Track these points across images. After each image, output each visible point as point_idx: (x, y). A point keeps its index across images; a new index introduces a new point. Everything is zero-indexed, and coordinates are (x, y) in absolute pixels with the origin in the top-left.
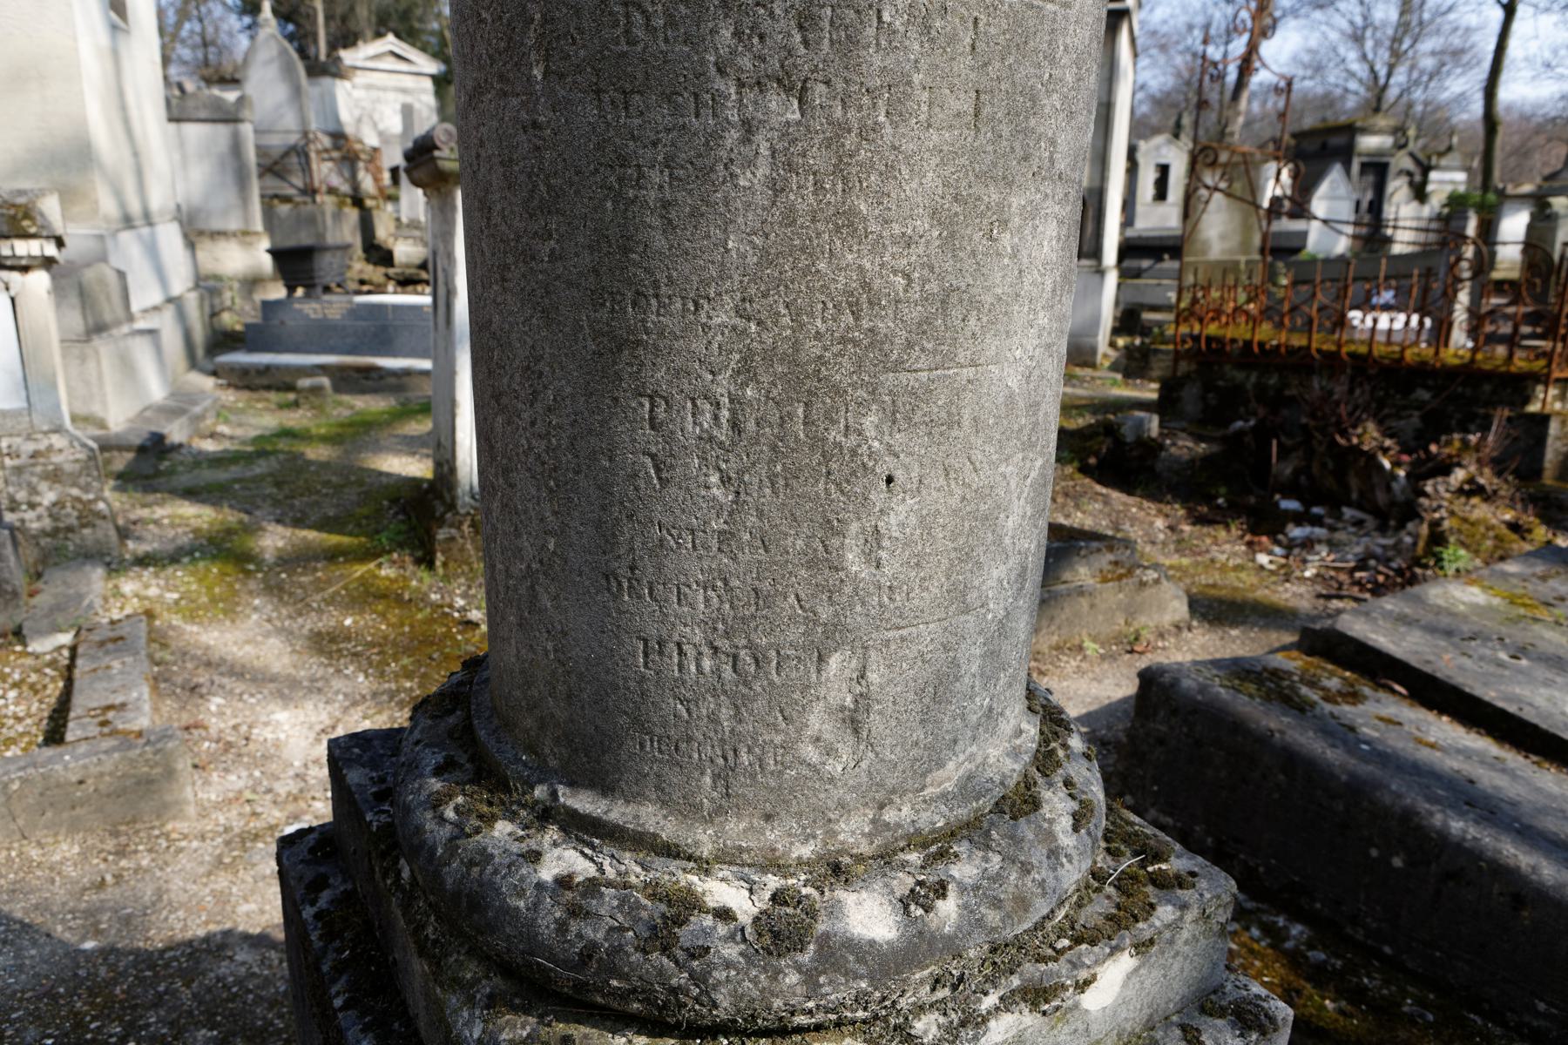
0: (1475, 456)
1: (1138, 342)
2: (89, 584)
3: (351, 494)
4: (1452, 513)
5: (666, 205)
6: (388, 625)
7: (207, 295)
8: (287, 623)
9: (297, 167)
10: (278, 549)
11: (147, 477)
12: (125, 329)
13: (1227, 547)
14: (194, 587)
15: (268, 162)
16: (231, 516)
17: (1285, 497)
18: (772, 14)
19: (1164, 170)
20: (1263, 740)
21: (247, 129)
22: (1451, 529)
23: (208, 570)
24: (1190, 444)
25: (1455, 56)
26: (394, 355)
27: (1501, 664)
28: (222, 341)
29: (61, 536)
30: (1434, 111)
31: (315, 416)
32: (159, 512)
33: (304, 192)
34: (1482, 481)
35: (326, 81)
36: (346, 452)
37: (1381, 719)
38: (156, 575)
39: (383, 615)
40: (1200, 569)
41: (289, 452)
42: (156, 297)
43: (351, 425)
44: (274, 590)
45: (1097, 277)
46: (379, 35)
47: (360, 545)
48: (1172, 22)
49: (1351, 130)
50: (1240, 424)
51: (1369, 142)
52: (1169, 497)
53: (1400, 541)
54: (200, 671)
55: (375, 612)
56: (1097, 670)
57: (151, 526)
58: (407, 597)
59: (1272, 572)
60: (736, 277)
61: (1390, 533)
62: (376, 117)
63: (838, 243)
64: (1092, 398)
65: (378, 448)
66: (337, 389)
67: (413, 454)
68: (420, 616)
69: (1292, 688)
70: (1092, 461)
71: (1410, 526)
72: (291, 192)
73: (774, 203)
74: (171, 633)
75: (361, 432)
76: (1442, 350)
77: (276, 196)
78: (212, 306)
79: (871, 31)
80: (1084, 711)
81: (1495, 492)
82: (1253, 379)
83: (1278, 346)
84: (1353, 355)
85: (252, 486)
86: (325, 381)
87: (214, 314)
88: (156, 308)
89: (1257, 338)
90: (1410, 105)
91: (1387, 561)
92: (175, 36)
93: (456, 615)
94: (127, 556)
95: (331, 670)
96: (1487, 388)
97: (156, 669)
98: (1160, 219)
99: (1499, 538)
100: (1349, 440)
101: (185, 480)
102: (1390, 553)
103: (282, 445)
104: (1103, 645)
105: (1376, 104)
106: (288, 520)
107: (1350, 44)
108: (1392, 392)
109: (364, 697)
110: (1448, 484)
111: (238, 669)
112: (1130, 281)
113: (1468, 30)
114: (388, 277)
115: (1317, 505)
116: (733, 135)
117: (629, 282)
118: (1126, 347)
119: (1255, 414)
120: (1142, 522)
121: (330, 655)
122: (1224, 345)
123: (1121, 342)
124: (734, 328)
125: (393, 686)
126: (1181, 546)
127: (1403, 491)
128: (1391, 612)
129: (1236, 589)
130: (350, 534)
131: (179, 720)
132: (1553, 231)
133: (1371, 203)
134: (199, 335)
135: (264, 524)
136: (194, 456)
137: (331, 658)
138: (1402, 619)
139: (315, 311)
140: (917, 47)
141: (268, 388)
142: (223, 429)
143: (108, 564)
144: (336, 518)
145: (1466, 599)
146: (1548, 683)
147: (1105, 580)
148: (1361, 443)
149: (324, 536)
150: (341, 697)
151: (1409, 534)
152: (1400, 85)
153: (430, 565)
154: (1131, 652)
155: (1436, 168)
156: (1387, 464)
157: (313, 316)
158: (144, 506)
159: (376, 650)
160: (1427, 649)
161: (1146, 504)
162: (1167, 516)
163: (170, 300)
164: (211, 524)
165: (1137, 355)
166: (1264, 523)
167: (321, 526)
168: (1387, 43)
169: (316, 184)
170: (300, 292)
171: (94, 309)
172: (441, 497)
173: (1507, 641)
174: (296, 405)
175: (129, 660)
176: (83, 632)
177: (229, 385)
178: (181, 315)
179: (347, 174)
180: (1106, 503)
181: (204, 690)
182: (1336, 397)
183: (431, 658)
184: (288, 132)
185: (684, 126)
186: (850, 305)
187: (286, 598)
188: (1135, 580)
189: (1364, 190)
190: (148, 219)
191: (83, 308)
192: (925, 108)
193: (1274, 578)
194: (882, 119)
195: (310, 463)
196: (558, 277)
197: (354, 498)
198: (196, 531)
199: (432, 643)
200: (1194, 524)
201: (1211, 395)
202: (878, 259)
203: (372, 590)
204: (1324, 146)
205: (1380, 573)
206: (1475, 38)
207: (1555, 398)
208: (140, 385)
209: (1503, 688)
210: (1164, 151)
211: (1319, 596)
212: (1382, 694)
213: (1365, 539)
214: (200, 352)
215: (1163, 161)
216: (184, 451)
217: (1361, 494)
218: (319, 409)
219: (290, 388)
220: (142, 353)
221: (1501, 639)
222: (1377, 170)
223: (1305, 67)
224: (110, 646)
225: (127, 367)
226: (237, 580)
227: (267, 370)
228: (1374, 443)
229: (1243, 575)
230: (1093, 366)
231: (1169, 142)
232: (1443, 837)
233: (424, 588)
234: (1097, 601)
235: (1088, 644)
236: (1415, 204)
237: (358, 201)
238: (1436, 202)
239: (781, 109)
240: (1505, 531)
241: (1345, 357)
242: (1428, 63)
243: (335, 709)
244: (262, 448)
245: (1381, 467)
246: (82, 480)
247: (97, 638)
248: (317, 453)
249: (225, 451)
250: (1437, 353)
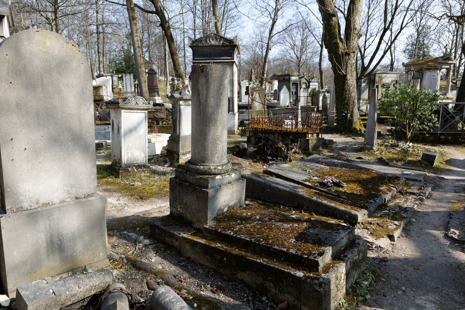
20: (255, 180)
49: (289, 75)
98: (245, 99)
123: (240, 129)
204: (284, 79)
230: (234, 134)
232: (273, 186)
239: (214, 127)
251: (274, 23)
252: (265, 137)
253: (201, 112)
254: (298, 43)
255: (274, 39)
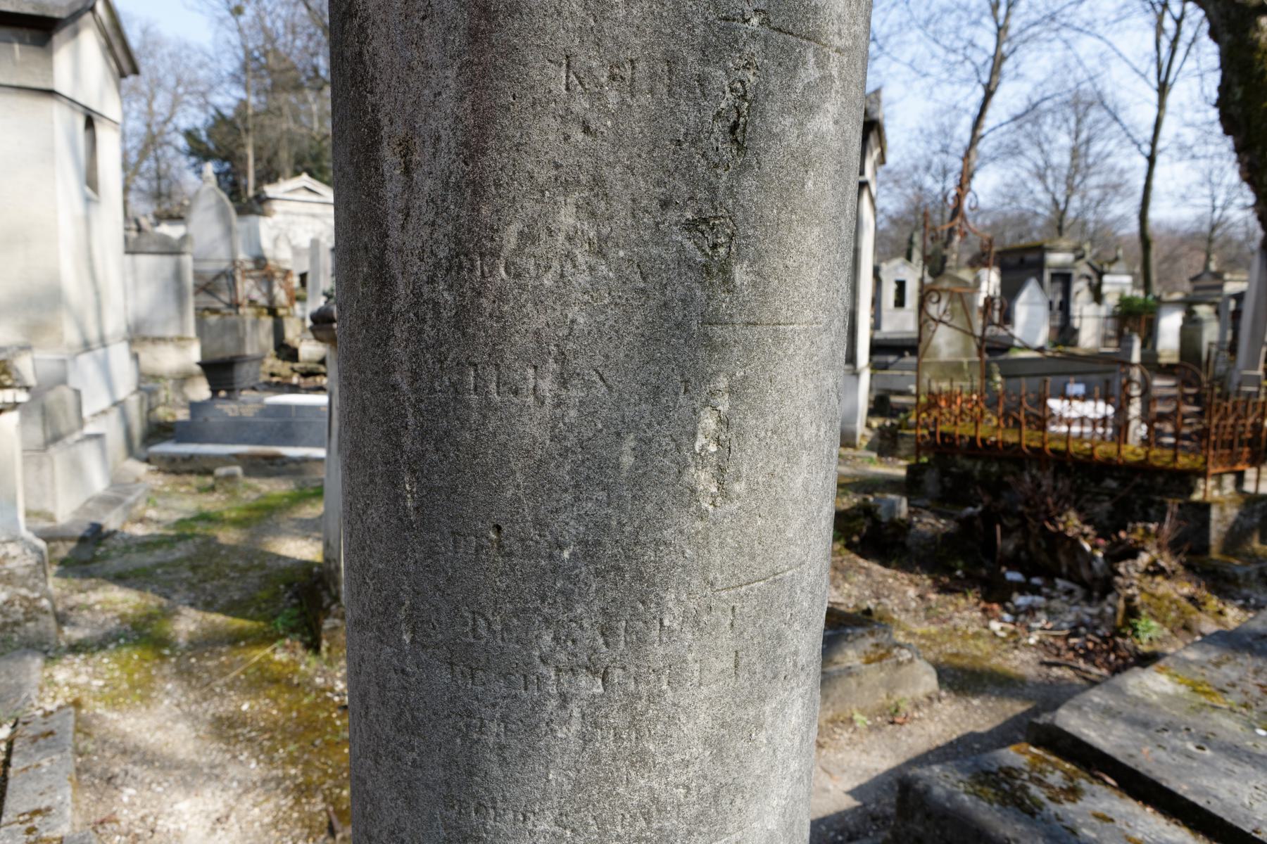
0: (1155, 541)
1: (888, 423)
2: (28, 675)
3: (254, 577)
4: (1142, 590)
5: (502, 747)
6: (279, 710)
7: (145, 395)
8: (193, 708)
9: (226, 287)
10: (190, 633)
11: (85, 563)
12: (77, 436)
13: (966, 613)
14: (117, 674)
15: (202, 283)
16: (152, 601)
17: (1010, 569)
18: (581, 627)
19: (901, 286)
21: (187, 260)
22: (1142, 604)
23: (130, 657)
24: (932, 521)
25: (1114, 189)
26: (295, 445)
27: (1189, 756)
28: (158, 431)
29: (9, 629)
30: (1102, 229)
31: (228, 500)
32: (93, 597)
33: (230, 306)
34: (1162, 563)
35: (252, 219)
36: (252, 536)
37: (1097, 816)
38: (86, 662)
39: (275, 700)
40: (946, 637)
41: (205, 536)
42: (104, 402)
43: (257, 508)
44: (185, 673)
45: (853, 378)
46: (297, 173)
47: (259, 630)
48: (902, 164)
49: (1040, 250)
50: (970, 510)
51: (1056, 259)
52: (918, 569)
53: (1103, 611)
54: (117, 759)
55: (268, 697)
56: (866, 741)
57: (85, 612)
58: (296, 681)
59: (1004, 640)
60: (555, 799)
61: (1094, 603)
62: (291, 235)
63: (633, 773)
64: (855, 476)
65: (278, 532)
66: (247, 473)
67: (307, 537)
68: (306, 701)
69: (1024, 789)
70: (856, 539)
71: (1110, 598)
72: (219, 305)
73: (584, 749)
74: (95, 722)
75: (264, 517)
76: (1123, 446)
77: (207, 309)
78: (150, 404)
79: (655, 633)
80: (856, 784)
81: (1174, 572)
82: (979, 466)
83: (996, 442)
84: (1054, 451)
85: (171, 570)
86: (238, 470)
87: (151, 409)
88: (104, 412)
89: (980, 434)
90: (1085, 223)
91: (1093, 629)
92: (136, 171)
93: (336, 699)
94: (63, 644)
95: (228, 756)
96: (1160, 480)
97: (79, 760)
98: (901, 323)
99: (1182, 612)
100: (1056, 526)
101: (115, 565)
102: (1096, 622)
103: (200, 528)
104: (870, 717)
105: (1059, 224)
106: (200, 604)
107: (1036, 180)
108: (1087, 480)
109: (254, 783)
110: (1136, 566)
111: (149, 757)
112: (879, 372)
113: (1122, 172)
114: (293, 370)
115: (1035, 576)
116: (553, 704)
117: (473, 796)
118: (880, 428)
119: (981, 501)
120: (897, 592)
121: (228, 740)
122: (954, 440)
124: (554, 834)
125: (280, 773)
126: (930, 613)
127: (1102, 568)
128: (1098, 704)
129: (975, 657)
130: (251, 618)
131: (95, 813)
132: (1200, 331)
133: (1061, 303)
134: (137, 430)
135: (180, 607)
136: (125, 540)
137: (228, 744)
138: (1108, 712)
139: (233, 410)
140: (690, 636)
141: (191, 472)
142: (151, 513)
143: (46, 652)
144: (240, 602)
145: (1158, 688)
146: (1229, 774)
147: (869, 662)
148: (1066, 530)
149: (229, 619)
150: (235, 784)
151: (1110, 605)
152: (1076, 209)
153: (317, 650)
154: (893, 723)
155: (1108, 273)
156: (1087, 547)
157: (231, 414)
158: (80, 591)
159: (267, 736)
160: (1129, 743)
161: (900, 575)
162: (917, 585)
163: (116, 404)
164: (136, 609)
165: (888, 435)
166: (996, 594)
167: (226, 610)
168: (1063, 179)
169: (240, 299)
170: (223, 394)
171: (52, 422)
172: (327, 588)
173: (1193, 730)
174: (212, 489)
175: (57, 757)
176: (19, 726)
177: (159, 470)
178: (124, 415)
179: (264, 289)
180: (868, 575)
181: (119, 781)
182: (1044, 489)
183: (313, 744)
184: (220, 260)
185: (516, 696)
186: (643, 814)
187: (194, 682)
188: (894, 660)
189: (1055, 293)
190: (103, 342)
191: (44, 424)
192: (697, 674)
193: (1005, 646)
194: (665, 687)
195: (221, 546)
196: (418, 779)
197: (256, 581)
198: (123, 616)
199: (315, 729)
200: (939, 593)
201: (947, 479)
202: (664, 780)
203: (267, 675)
204: (1022, 261)
205: (1089, 640)
206: (1127, 176)
207: (1213, 487)
208: (87, 481)
209: (1193, 780)
210: (901, 270)
211: (1042, 663)
212: (1097, 787)
213: (1076, 608)
214: (137, 442)
215: (900, 278)
216: (117, 537)
217: (1070, 569)
218: (232, 494)
219: (209, 472)
220: (90, 456)
221: (1188, 729)
222: (1064, 278)
223: (1004, 196)
224: (42, 742)
225: (76, 468)
226: (154, 665)
227: (191, 458)
228: (1076, 530)
229: (980, 643)
230: (854, 446)
231: (904, 264)
233: (311, 672)
234: (863, 680)
235: (857, 716)
236: (1094, 306)
237: (272, 311)
238: (1111, 300)
240: (1184, 602)
241: (1049, 453)
242: (1095, 194)
243: (229, 796)
244: (182, 532)
245: (1082, 549)
246: (30, 582)
247: (31, 733)
248: (228, 536)
249: (152, 536)
250: (1119, 451)
251: (989, 94)
252: (986, 474)
253: (393, 435)
254: (1061, 158)
255: (984, 147)
